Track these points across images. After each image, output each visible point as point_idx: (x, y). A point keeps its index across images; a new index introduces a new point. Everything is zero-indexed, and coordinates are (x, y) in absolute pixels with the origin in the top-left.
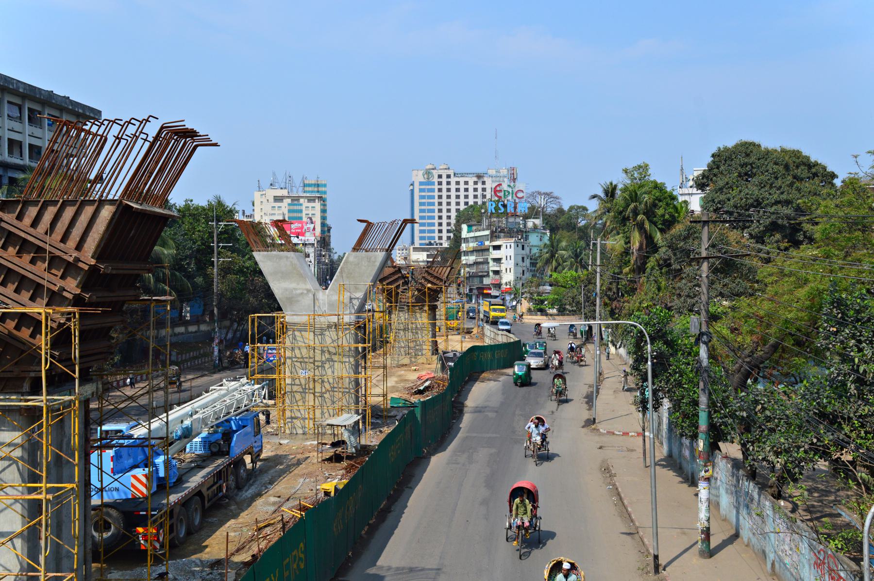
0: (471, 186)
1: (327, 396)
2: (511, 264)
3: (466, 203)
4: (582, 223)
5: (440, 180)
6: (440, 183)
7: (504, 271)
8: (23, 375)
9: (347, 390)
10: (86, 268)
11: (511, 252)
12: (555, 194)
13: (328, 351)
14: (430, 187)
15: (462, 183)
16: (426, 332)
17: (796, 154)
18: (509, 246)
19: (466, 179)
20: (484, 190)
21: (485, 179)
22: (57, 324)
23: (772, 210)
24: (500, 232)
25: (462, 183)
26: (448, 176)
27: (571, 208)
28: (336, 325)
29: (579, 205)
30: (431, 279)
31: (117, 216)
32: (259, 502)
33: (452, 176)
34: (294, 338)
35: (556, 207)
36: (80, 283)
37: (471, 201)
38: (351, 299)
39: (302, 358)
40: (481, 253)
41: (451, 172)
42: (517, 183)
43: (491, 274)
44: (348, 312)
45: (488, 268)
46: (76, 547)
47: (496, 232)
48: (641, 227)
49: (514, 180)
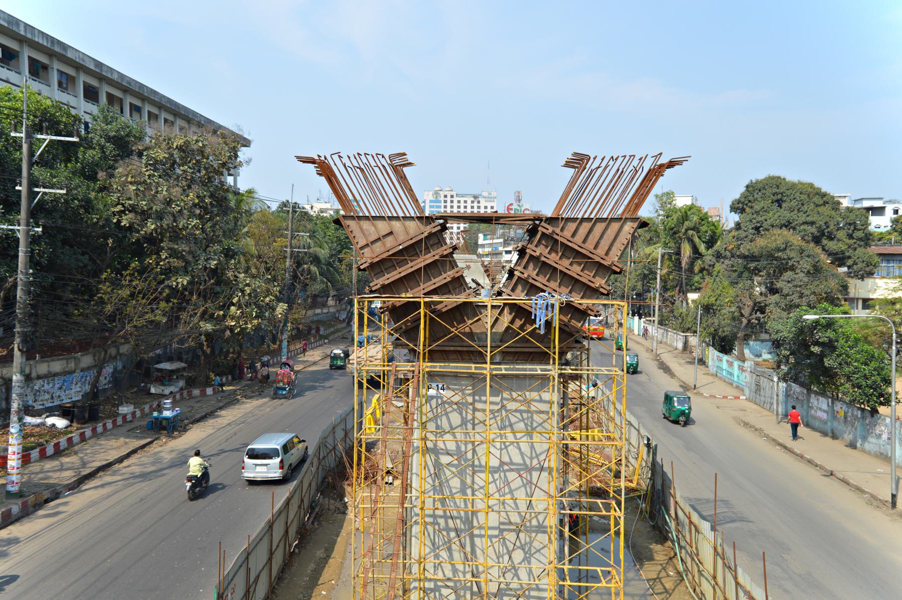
6: (445, 202)
15: (462, 202)
17: (811, 185)
19: (465, 199)
21: (480, 199)
23: (802, 227)
25: (462, 202)
26: (452, 196)
33: (455, 196)
40: (495, 256)
41: (454, 193)
48: (691, 241)
49: (519, 200)
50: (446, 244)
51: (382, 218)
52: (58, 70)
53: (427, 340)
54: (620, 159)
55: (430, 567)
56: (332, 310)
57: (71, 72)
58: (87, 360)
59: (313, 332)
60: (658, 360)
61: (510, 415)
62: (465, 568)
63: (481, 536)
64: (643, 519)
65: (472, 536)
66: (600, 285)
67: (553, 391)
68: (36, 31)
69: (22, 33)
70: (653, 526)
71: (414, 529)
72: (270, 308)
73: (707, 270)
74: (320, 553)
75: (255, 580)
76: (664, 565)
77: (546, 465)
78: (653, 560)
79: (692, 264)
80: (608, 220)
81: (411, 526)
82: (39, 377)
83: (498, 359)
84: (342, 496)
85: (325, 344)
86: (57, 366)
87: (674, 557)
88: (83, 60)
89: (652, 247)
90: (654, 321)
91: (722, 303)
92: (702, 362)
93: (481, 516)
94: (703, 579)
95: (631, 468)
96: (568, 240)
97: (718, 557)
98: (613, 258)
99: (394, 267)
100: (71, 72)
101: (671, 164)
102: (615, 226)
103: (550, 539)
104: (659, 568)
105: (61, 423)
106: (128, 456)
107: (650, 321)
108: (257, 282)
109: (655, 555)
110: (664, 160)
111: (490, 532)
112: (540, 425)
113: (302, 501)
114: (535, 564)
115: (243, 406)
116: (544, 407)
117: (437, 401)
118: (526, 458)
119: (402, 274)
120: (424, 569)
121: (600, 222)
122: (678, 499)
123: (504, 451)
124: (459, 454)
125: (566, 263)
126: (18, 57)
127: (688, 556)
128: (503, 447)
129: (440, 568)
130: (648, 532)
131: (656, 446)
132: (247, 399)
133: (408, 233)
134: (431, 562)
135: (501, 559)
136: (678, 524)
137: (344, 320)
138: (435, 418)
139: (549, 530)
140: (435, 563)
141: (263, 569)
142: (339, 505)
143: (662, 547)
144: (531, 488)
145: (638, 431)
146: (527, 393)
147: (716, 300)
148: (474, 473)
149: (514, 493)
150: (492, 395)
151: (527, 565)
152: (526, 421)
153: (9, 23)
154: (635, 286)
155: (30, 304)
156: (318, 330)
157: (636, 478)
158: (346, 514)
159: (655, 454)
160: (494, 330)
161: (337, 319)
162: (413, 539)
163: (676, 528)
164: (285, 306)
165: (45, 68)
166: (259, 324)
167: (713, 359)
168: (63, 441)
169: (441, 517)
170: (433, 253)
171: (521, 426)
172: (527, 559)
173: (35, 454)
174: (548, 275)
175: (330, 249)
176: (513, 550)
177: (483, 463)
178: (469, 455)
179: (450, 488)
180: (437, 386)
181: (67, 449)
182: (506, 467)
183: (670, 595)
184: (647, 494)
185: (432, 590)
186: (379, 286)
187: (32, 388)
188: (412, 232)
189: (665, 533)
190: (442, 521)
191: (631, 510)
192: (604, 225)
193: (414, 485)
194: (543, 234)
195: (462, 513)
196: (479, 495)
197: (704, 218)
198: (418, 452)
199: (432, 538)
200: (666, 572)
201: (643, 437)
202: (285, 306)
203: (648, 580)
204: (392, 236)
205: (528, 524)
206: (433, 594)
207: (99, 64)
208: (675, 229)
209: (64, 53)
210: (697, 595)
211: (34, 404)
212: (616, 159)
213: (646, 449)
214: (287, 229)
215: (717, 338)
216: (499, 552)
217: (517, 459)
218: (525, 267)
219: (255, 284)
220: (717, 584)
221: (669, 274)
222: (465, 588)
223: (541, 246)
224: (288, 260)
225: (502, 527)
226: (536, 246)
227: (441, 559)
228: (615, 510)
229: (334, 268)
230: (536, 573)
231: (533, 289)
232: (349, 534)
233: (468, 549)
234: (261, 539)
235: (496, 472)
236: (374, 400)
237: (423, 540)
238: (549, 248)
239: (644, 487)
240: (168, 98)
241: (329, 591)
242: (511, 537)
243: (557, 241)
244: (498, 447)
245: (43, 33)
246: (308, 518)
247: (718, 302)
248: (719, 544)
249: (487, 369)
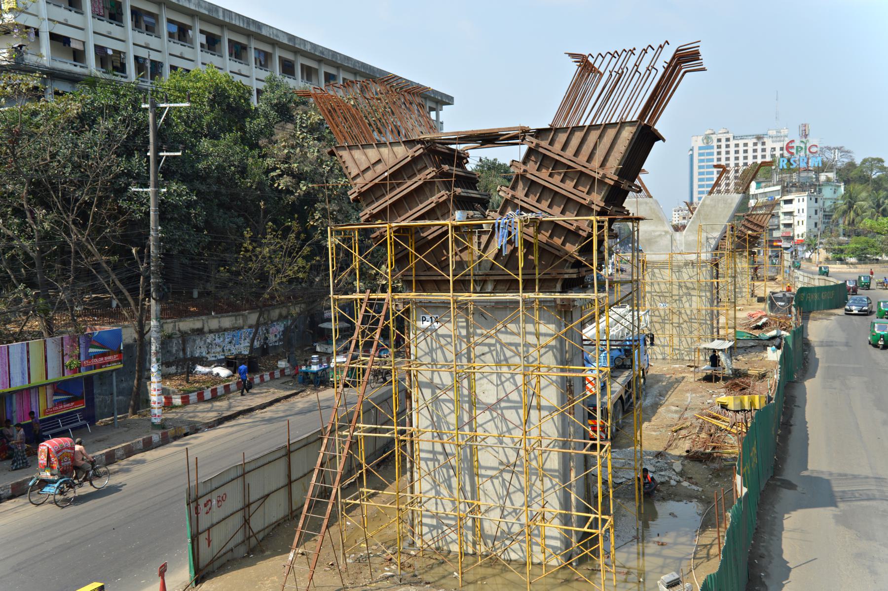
0: (750, 148)
1: (685, 325)
2: (803, 217)
3: (745, 164)
4: (875, 175)
5: (719, 144)
6: (719, 147)
7: (796, 223)
8: (558, 276)
9: (704, 322)
10: (612, 183)
11: (804, 205)
12: (846, 148)
13: (686, 286)
14: (709, 151)
15: (741, 145)
16: (746, 276)
18: (801, 200)
20: (764, 150)
21: (765, 140)
22: (587, 233)
24: (792, 187)
25: (741, 145)
26: (728, 140)
27: (865, 161)
28: (693, 263)
29: (874, 157)
30: (751, 227)
31: (636, 136)
32: (662, 410)
33: (731, 139)
34: (653, 274)
35: (846, 160)
36: (603, 197)
37: (750, 161)
38: (707, 238)
39: (661, 292)
41: (730, 136)
42: (808, 138)
43: (782, 227)
44: (705, 250)
45: (779, 221)
46: (609, 420)
47: (787, 187)
49: (806, 136)
52: (255, 49)
57: (267, 48)
58: (253, 318)
61: (504, 349)
68: (233, 15)
69: (221, 18)
80: (602, 127)
82: (211, 332)
86: (227, 322)
88: (277, 36)
100: (267, 48)
105: (224, 372)
106: (271, 403)
123: (500, 387)
126: (220, 41)
128: (499, 383)
153: (209, 10)
155: (160, 258)
165: (244, 48)
168: (220, 388)
173: (193, 397)
174: (538, 195)
181: (224, 395)
186: (367, 216)
187: (205, 341)
188: (400, 156)
206: (436, 531)
207: (292, 38)
209: (259, 32)
211: (207, 356)
227: (442, 496)
233: (468, 488)
238: (539, 163)
240: (362, 63)
245: (239, 15)
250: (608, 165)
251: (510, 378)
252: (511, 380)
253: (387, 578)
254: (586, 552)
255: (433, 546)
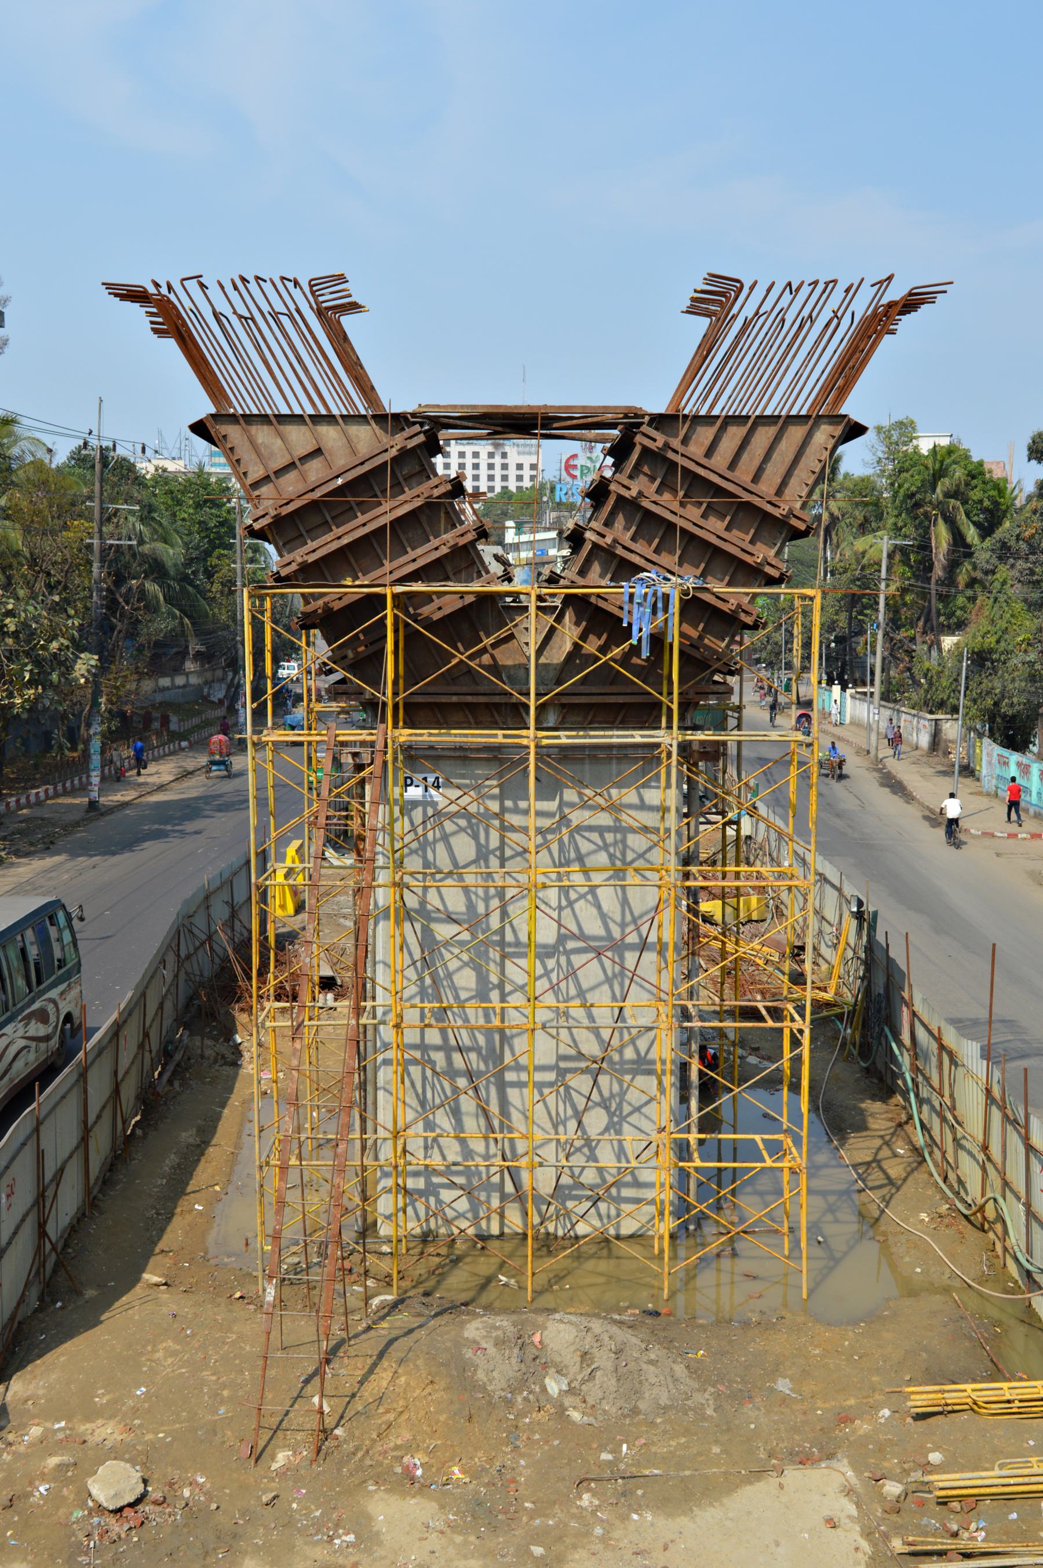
0: (483, 461)
15: (469, 455)
19: (476, 448)
20: (505, 467)
25: (469, 455)
48: (951, 522)
50: (436, 475)
51: (296, 419)
53: (401, 682)
54: (806, 290)
55: (416, 1145)
56: (194, 680)
59: (156, 725)
60: (880, 771)
61: (577, 837)
62: (487, 1147)
63: (520, 1085)
64: (848, 1058)
65: (502, 1087)
66: (765, 559)
67: (668, 786)
70: (867, 1069)
71: (381, 1074)
72: (61, 664)
73: (980, 582)
74: (188, 1136)
75: (55, 1176)
76: (887, 1138)
77: (653, 938)
78: (866, 1129)
79: (953, 566)
80: (781, 421)
81: (376, 1070)
83: (552, 719)
84: (228, 1030)
85: (183, 749)
87: (906, 1123)
89: (869, 539)
90: (872, 694)
91: (1010, 648)
92: (968, 771)
93: (520, 1044)
94: (963, 1155)
95: (824, 967)
96: (695, 524)
97: (994, 1109)
98: (792, 500)
99: (325, 527)
101: (911, 303)
102: (796, 434)
103: (660, 1083)
104: (878, 1142)
107: (865, 694)
108: (31, 608)
109: (870, 1119)
110: (895, 293)
111: (539, 1077)
112: (641, 856)
113: (146, 1035)
114: (629, 1134)
115: (12, 871)
116: (649, 819)
117: (425, 812)
118: (612, 925)
119: (345, 541)
120: (405, 1151)
121: (764, 425)
122: (918, 1007)
124: (473, 921)
125: (694, 513)
127: (934, 1115)
128: (564, 903)
129: (436, 1150)
130: (857, 1080)
131: (875, 914)
132: (18, 856)
133: (354, 452)
134: (417, 1136)
135: (561, 1129)
136: (916, 1056)
137: (221, 701)
138: (424, 845)
139: (658, 1067)
140: (426, 1139)
141: (70, 1157)
142: (223, 1048)
143: (884, 1106)
144: (622, 985)
145: (839, 890)
146: (614, 792)
147: (998, 642)
148: (504, 957)
149: (588, 996)
150: (539, 797)
151: (613, 1137)
152: (611, 850)
154: (834, 622)
156: (165, 721)
157: (833, 983)
158: (240, 1066)
159: (872, 928)
160: (543, 660)
161: (206, 699)
162: (381, 1094)
163: (912, 1064)
164: (93, 660)
166: (38, 698)
167: (990, 763)
169: (437, 1048)
170: (408, 494)
171: (602, 858)
172: (614, 1126)
174: (657, 541)
175: (186, 545)
176: (585, 1110)
177: (524, 938)
178: (495, 922)
179: (456, 989)
180: (425, 779)
182: (571, 945)
183: (898, 1189)
184: (854, 1010)
185: (421, 1193)
189: (889, 1081)
190: (439, 1057)
191: (823, 1043)
192: (771, 431)
193: (379, 979)
194: (645, 450)
195: (481, 1040)
196: (517, 999)
197: (976, 473)
198: (387, 917)
199: (420, 1091)
200: (891, 1149)
201: (849, 902)
202: (93, 660)
203: (855, 1166)
204: (321, 459)
205: (616, 1057)
208: (918, 496)
210: (951, 1187)
212: (798, 290)
213: (854, 923)
214: (90, 498)
215: (999, 720)
216: (558, 1113)
217: (593, 927)
218: (608, 523)
219: (25, 611)
220: (989, 1159)
221: (904, 591)
222: (488, 1187)
223: (642, 476)
224: (96, 565)
225: (563, 1065)
226: (631, 477)
227: (438, 1131)
228: (793, 1020)
229: (196, 587)
230: (631, 1149)
231: (625, 570)
232: (247, 1102)
233: (494, 1108)
234: (63, 1097)
235: (550, 955)
236: (291, 851)
237: (400, 1096)
238: (658, 481)
239: (849, 998)
241: (209, 1204)
242: (581, 1083)
243: (674, 465)
244: (554, 903)
246: (160, 1074)
247: (1003, 644)
248: (995, 1080)
249: (529, 737)
250: (788, 492)
251: (587, 894)
252: (589, 897)
253: (394, 1306)
254: (702, 1207)
255: (471, 1231)
